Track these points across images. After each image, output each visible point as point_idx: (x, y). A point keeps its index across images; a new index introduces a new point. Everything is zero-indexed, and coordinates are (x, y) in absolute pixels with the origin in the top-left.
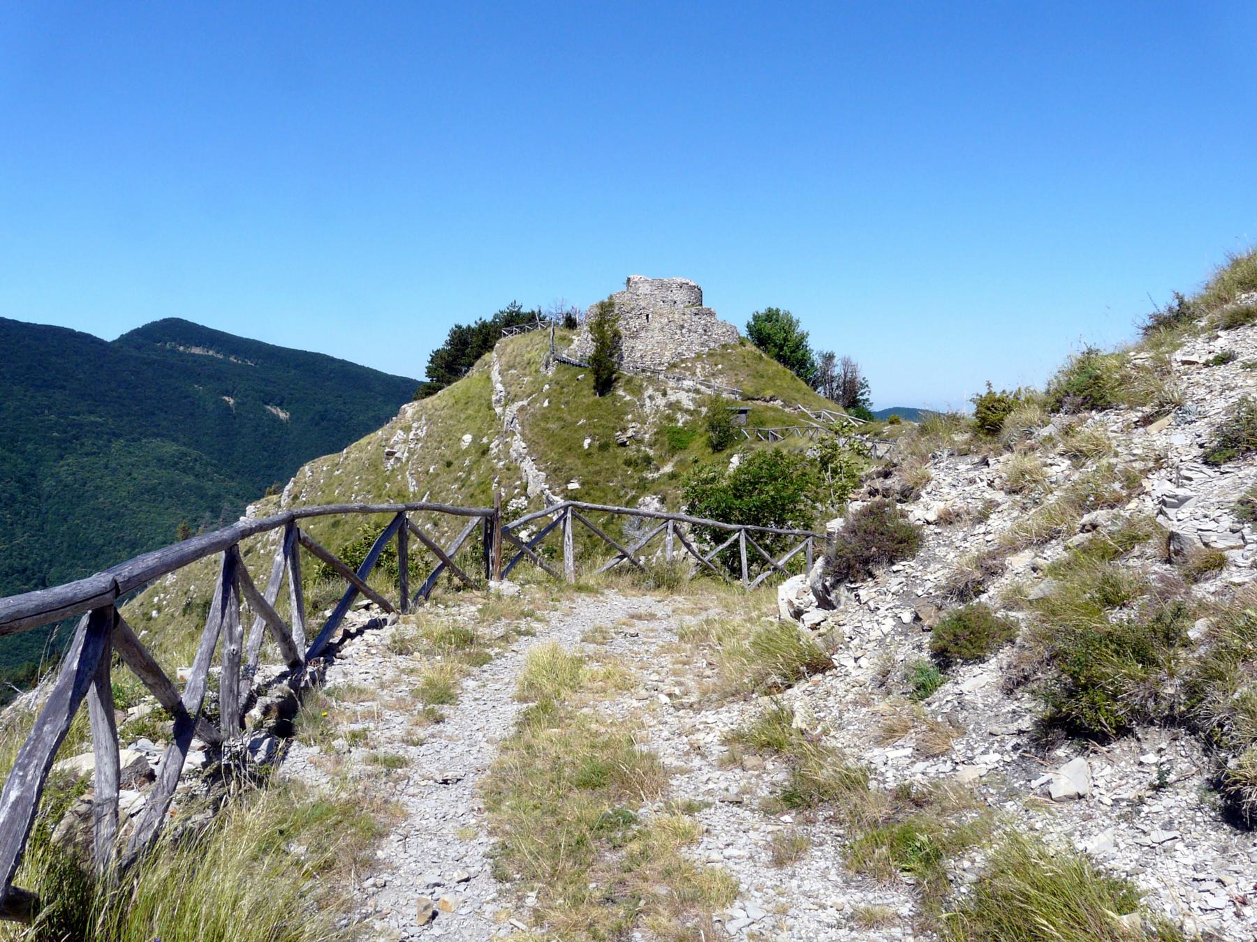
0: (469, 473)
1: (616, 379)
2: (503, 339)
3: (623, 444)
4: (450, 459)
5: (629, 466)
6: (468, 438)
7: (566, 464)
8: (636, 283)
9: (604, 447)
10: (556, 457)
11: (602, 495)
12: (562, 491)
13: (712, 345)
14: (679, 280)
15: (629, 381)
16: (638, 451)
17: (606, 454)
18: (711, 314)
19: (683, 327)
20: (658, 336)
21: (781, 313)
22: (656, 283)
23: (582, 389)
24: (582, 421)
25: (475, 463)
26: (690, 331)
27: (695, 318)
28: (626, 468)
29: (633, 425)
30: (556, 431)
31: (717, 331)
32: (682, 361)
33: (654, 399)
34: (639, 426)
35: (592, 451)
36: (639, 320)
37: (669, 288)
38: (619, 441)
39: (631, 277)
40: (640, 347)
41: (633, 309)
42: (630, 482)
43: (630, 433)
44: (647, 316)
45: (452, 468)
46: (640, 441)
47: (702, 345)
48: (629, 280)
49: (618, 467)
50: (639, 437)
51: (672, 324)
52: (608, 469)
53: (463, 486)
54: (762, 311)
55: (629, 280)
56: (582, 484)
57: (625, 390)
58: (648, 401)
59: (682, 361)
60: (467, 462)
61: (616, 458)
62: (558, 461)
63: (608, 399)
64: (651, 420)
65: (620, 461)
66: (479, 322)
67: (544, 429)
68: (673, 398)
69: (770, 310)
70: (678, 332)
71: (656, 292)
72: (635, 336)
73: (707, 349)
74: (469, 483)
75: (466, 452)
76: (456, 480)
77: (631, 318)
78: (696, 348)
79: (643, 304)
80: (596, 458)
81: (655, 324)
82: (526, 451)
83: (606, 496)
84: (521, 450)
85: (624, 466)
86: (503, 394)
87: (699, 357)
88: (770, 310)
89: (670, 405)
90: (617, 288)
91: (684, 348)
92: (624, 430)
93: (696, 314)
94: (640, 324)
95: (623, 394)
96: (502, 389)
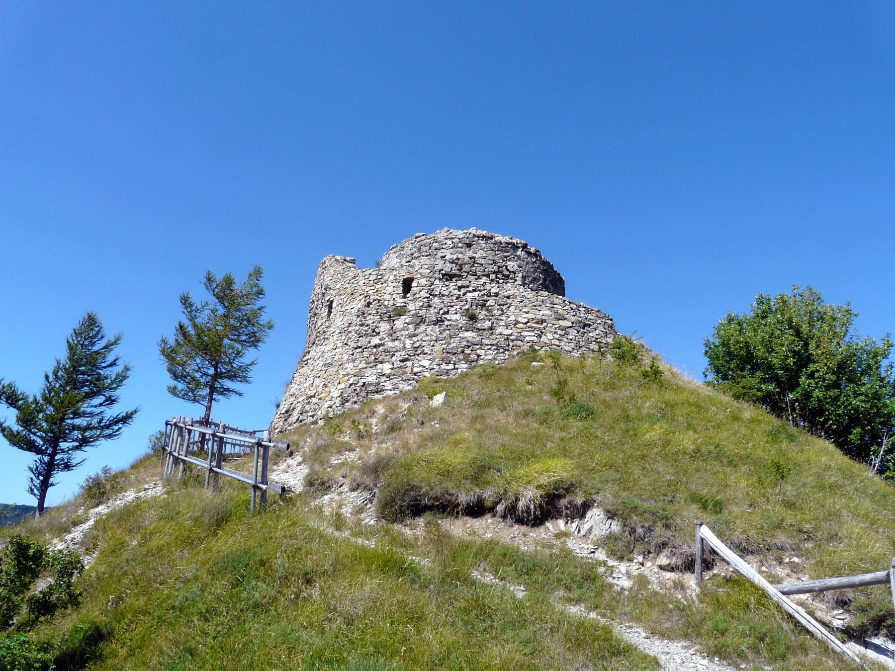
93: (449, 277)
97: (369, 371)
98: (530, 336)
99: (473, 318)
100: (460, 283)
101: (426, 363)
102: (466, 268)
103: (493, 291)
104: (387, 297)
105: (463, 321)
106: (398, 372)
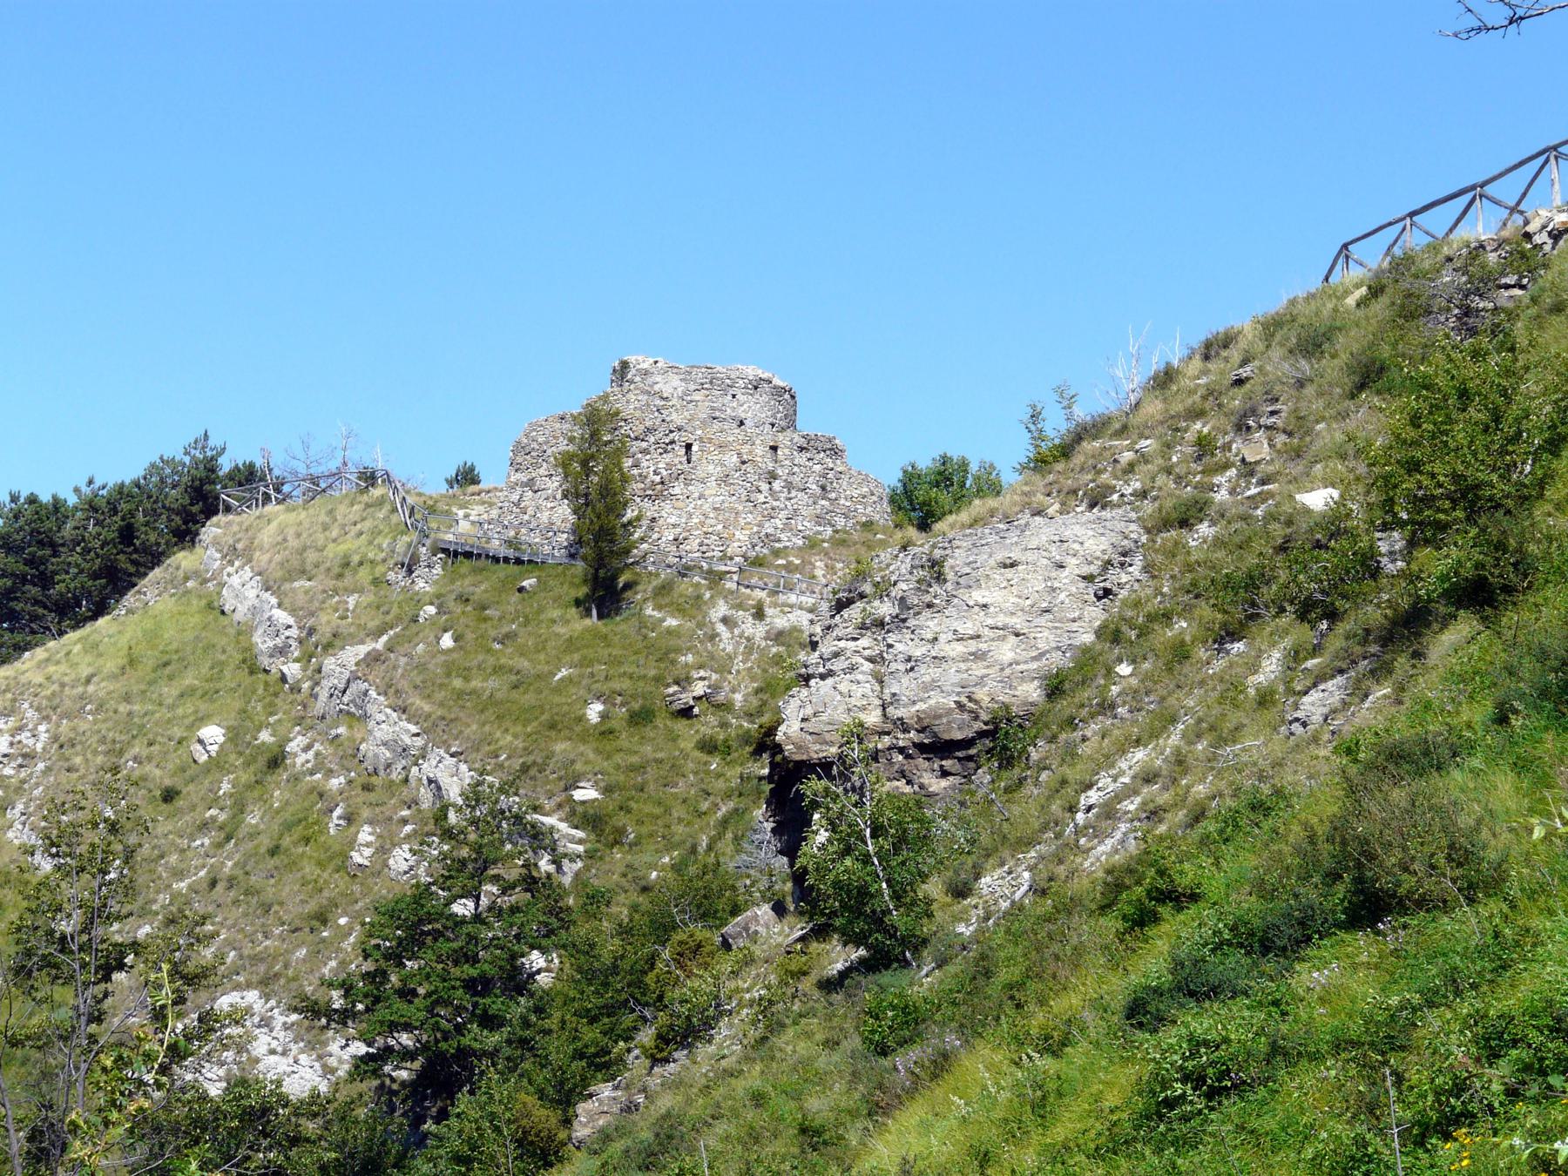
0: (240, 808)
1: (628, 586)
2: (220, 518)
3: (686, 713)
4: (168, 782)
5: (710, 753)
6: (213, 733)
7: (553, 753)
8: (646, 373)
9: (640, 718)
10: (519, 744)
11: (658, 811)
12: (560, 806)
13: (840, 522)
14: (752, 371)
15: (664, 589)
16: (724, 725)
17: (649, 732)
18: (835, 452)
19: (772, 476)
20: (715, 494)
21: (974, 468)
22: (699, 376)
23: (541, 610)
24: (564, 672)
25: (249, 787)
26: (789, 486)
27: (801, 459)
28: (704, 757)
29: (702, 673)
30: (499, 695)
31: (848, 491)
32: (777, 553)
33: (736, 625)
34: (714, 676)
35: (614, 724)
36: (668, 457)
37: (727, 387)
38: (677, 706)
39: (632, 359)
40: (672, 520)
41: (649, 430)
42: (720, 784)
43: (699, 689)
44: (689, 447)
45: (180, 803)
46: (726, 707)
47: (819, 519)
48: (625, 365)
49: (686, 757)
50: (721, 698)
51: (749, 467)
52: (661, 761)
53: (228, 838)
54: (926, 462)
55: (625, 365)
56: (607, 790)
57: (659, 607)
58: (721, 628)
59: (777, 553)
60: (226, 787)
61: (674, 740)
62: (527, 751)
63: (620, 626)
64: (738, 665)
65: (688, 744)
66: (86, 490)
67: (460, 694)
68: (781, 623)
69: (945, 460)
70: (764, 487)
71: (697, 396)
72: (659, 492)
73: (829, 530)
74: (242, 832)
75: (217, 764)
76: (204, 826)
77: (645, 452)
78: (806, 525)
79: (677, 419)
80: (624, 740)
81: (708, 466)
82: (419, 742)
83: (668, 811)
84: (408, 740)
85: (697, 754)
86: (294, 632)
87: (812, 544)
88: (945, 460)
89: (778, 636)
90: (591, 385)
91: (779, 524)
92: (683, 682)
93: (802, 449)
94: (669, 466)
95: (656, 614)
96: (291, 621)
97: (767, 525)
98: (860, 508)
99: (823, 488)
100: (808, 455)
101: (808, 524)
102: (812, 443)
103: (831, 465)
104: (759, 459)
105: (819, 491)
106: (787, 527)
